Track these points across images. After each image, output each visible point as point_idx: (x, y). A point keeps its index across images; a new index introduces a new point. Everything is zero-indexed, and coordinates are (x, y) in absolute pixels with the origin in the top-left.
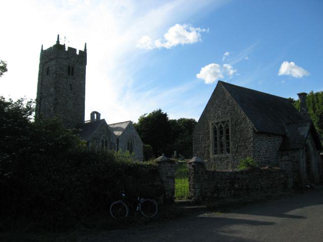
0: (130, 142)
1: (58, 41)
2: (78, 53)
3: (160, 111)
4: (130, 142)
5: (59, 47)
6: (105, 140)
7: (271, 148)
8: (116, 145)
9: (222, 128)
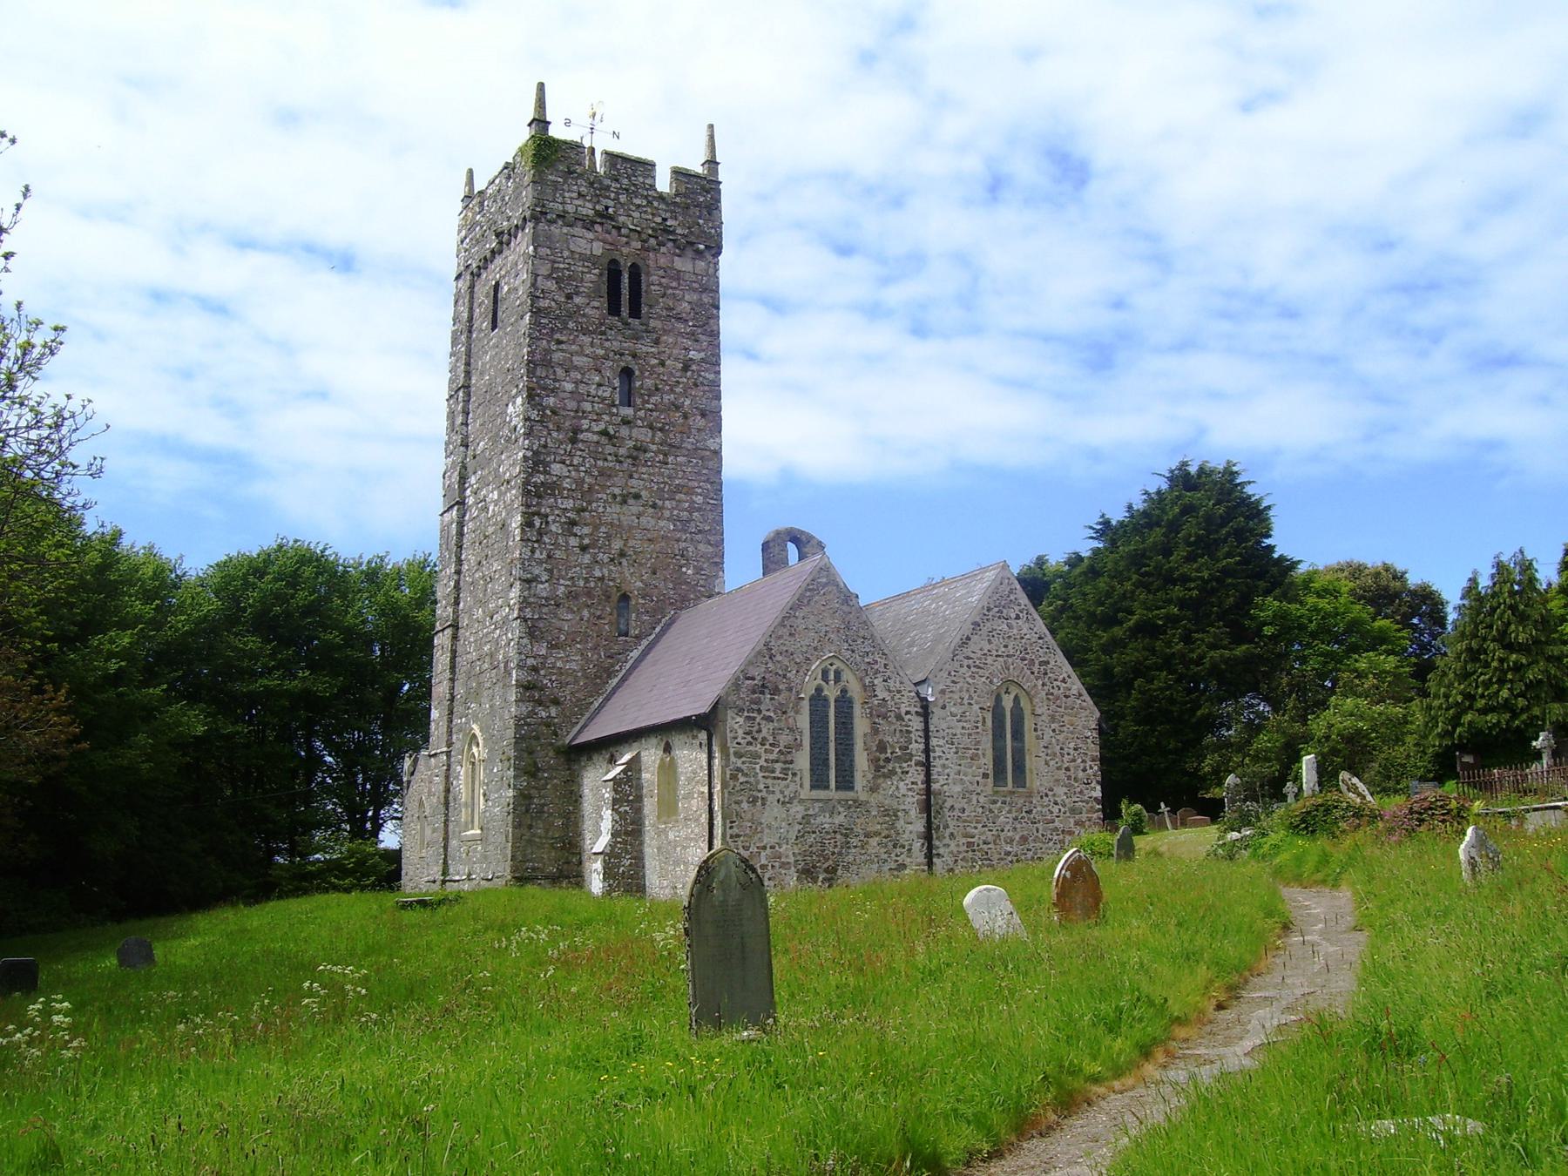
0: (1008, 702)
1: (540, 122)
2: (663, 183)
3: (118, 535)
4: (1008, 702)
5: (548, 154)
6: (831, 692)
8: (916, 724)
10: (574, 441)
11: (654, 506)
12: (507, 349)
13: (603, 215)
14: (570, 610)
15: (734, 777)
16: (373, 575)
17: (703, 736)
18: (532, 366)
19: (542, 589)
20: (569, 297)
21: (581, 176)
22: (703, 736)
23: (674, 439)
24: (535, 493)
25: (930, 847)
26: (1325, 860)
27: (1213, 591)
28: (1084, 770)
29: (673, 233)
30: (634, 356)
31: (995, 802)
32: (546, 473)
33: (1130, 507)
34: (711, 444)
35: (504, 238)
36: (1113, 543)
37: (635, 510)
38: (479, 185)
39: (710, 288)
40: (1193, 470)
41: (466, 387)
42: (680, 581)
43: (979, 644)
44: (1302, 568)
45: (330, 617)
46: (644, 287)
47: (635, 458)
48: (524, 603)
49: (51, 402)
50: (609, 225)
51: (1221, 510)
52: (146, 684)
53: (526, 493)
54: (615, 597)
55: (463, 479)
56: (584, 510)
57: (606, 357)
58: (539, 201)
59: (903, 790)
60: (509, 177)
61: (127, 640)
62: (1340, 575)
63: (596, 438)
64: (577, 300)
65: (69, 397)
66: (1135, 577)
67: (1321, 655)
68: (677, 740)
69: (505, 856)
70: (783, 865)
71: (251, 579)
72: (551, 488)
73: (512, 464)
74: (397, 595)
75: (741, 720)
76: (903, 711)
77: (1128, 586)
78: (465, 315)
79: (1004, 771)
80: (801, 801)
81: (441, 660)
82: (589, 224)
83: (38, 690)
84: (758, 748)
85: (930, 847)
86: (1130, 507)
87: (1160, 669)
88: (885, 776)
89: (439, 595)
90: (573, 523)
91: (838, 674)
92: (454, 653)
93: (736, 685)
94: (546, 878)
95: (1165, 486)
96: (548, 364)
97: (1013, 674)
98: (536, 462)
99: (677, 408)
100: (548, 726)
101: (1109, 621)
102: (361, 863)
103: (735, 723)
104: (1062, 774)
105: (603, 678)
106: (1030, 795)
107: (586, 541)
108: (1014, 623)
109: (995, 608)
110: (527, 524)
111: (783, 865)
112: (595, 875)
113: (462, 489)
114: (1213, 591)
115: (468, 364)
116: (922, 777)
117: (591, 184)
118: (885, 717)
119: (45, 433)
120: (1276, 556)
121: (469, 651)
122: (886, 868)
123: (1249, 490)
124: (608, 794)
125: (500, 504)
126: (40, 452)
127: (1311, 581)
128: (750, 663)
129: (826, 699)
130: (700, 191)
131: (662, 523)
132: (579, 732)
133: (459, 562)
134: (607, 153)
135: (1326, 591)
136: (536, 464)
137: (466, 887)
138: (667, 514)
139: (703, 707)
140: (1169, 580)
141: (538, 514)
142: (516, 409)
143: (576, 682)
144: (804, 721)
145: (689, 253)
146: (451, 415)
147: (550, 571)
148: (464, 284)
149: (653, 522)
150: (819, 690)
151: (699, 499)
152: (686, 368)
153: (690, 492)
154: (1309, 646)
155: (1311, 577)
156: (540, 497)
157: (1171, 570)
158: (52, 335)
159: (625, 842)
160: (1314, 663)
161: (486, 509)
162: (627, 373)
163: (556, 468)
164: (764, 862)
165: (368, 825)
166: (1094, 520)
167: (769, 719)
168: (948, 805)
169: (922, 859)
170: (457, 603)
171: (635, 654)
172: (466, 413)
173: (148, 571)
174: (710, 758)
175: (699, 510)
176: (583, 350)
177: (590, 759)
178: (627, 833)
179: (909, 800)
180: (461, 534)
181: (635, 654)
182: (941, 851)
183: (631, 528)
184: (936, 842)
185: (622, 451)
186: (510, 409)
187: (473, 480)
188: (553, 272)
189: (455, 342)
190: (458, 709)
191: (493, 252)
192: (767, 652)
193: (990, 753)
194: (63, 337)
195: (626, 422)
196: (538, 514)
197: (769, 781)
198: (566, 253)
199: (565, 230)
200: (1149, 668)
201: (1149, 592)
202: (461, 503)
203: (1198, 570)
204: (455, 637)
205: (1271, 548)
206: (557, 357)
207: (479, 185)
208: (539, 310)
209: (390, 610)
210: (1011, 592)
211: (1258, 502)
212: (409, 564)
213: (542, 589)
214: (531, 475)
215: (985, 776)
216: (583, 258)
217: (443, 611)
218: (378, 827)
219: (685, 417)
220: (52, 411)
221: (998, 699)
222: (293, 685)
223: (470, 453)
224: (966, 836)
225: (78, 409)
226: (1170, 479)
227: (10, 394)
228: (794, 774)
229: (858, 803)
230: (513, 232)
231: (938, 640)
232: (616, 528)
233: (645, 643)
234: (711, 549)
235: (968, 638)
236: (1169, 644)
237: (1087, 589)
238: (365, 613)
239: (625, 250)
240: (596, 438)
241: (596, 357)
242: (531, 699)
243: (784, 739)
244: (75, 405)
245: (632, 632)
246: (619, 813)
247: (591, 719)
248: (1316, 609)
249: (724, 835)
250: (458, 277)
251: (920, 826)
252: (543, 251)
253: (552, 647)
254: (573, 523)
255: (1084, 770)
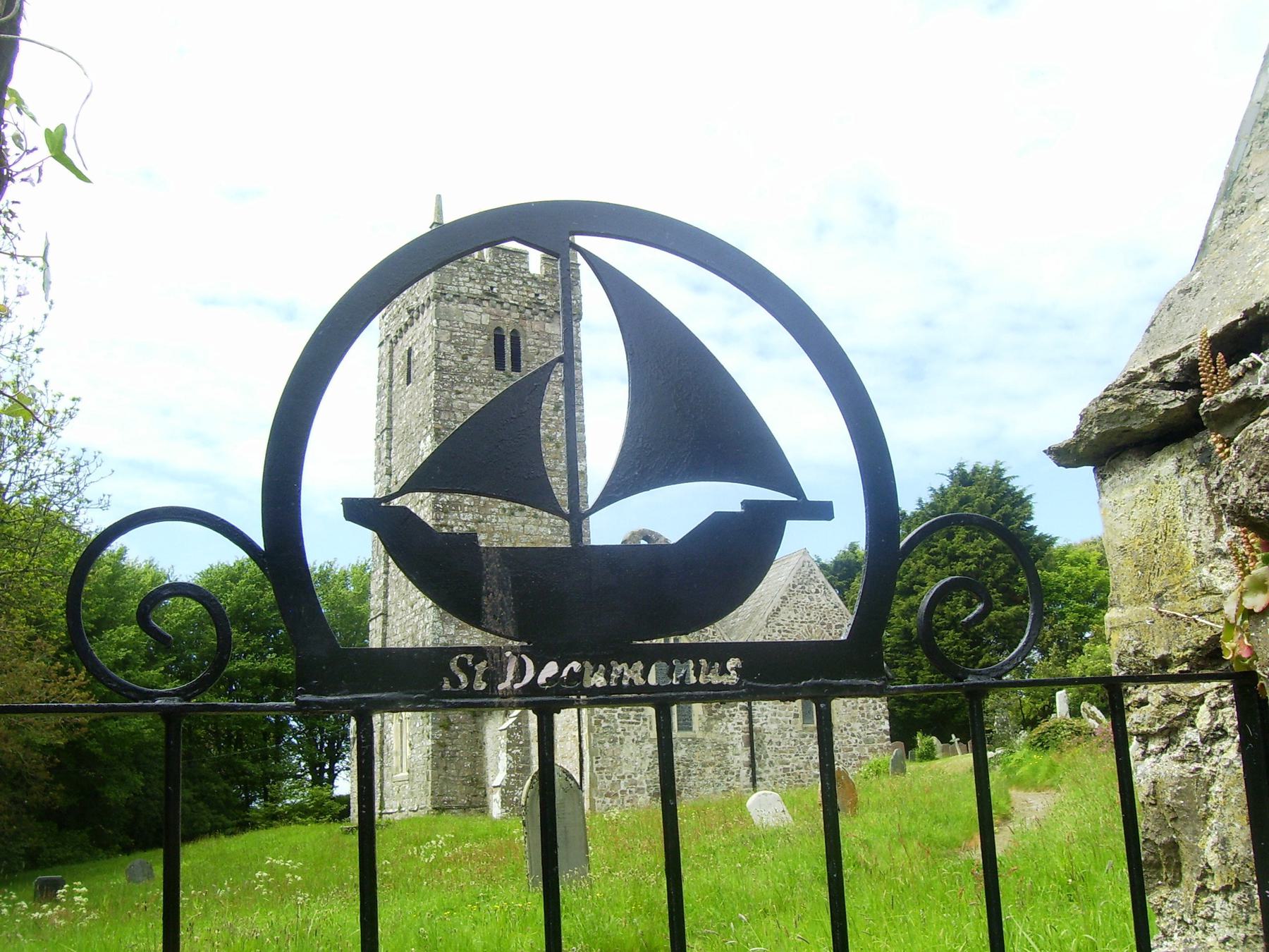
13: (490, 294)
15: (598, 723)
20: (465, 358)
25: (754, 773)
26: (1052, 768)
27: (987, 565)
28: (875, 709)
29: (544, 304)
31: (804, 736)
37: (520, 519)
40: (969, 469)
41: (389, 429)
44: (1059, 543)
46: (522, 348)
49: (71, 454)
51: (991, 500)
52: (147, 667)
56: (480, 521)
59: (731, 729)
61: (132, 633)
62: (1093, 547)
64: (471, 360)
65: (84, 450)
66: (926, 556)
67: (1077, 611)
69: (426, 792)
70: (638, 790)
71: (229, 583)
74: (343, 591)
77: (921, 563)
82: (478, 301)
83: (64, 673)
85: (754, 773)
86: (920, 501)
87: (948, 629)
88: (715, 718)
89: (372, 591)
94: (459, 808)
95: (946, 483)
99: (551, 440)
102: (319, 804)
104: (857, 712)
108: (814, 596)
111: (638, 790)
112: (495, 804)
114: (987, 565)
115: (390, 411)
116: (746, 718)
119: (66, 477)
120: (1037, 534)
122: (720, 790)
123: (1012, 483)
124: (504, 741)
126: (63, 492)
127: (1066, 553)
131: (542, 529)
135: (1078, 560)
137: (398, 817)
138: (545, 522)
140: (953, 558)
149: (535, 528)
154: (1066, 604)
155: (1065, 552)
156: (446, 513)
157: (954, 550)
158: (72, 404)
159: (518, 778)
160: (1071, 617)
164: (623, 788)
165: (326, 775)
168: (767, 739)
169: (748, 782)
170: (386, 596)
173: (148, 579)
177: (490, 713)
178: (518, 770)
179: (736, 736)
182: (763, 776)
183: (517, 534)
184: (758, 769)
186: (422, 445)
189: (379, 395)
191: (406, 325)
194: (78, 405)
197: (626, 726)
198: (462, 324)
199: (460, 306)
201: (938, 567)
203: (975, 548)
204: (385, 623)
205: (1032, 529)
206: (457, 404)
208: (442, 369)
210: (811, 572)
211: (1022, 492)
215: (796, 716)
216: (475, 327)
217: (375, 603)
218: (333, 776)
220: (71, 461)
222: (265, 666)
223: (393, 480)
224: (782, 763)
225: (91, 459)
226: (952, 477)
227: (41, 449)
228: (645, 720)
229: (696, 741)
230: (420, 310)
235: (778, 609)
236: (954, 608)
239: (507, 320)
244: (88, 456)
246: (512, 755)
248: (1070, 575)
249: (591, 767)
251: (745, 757)
252: (444, 323)
255: (875, 709)
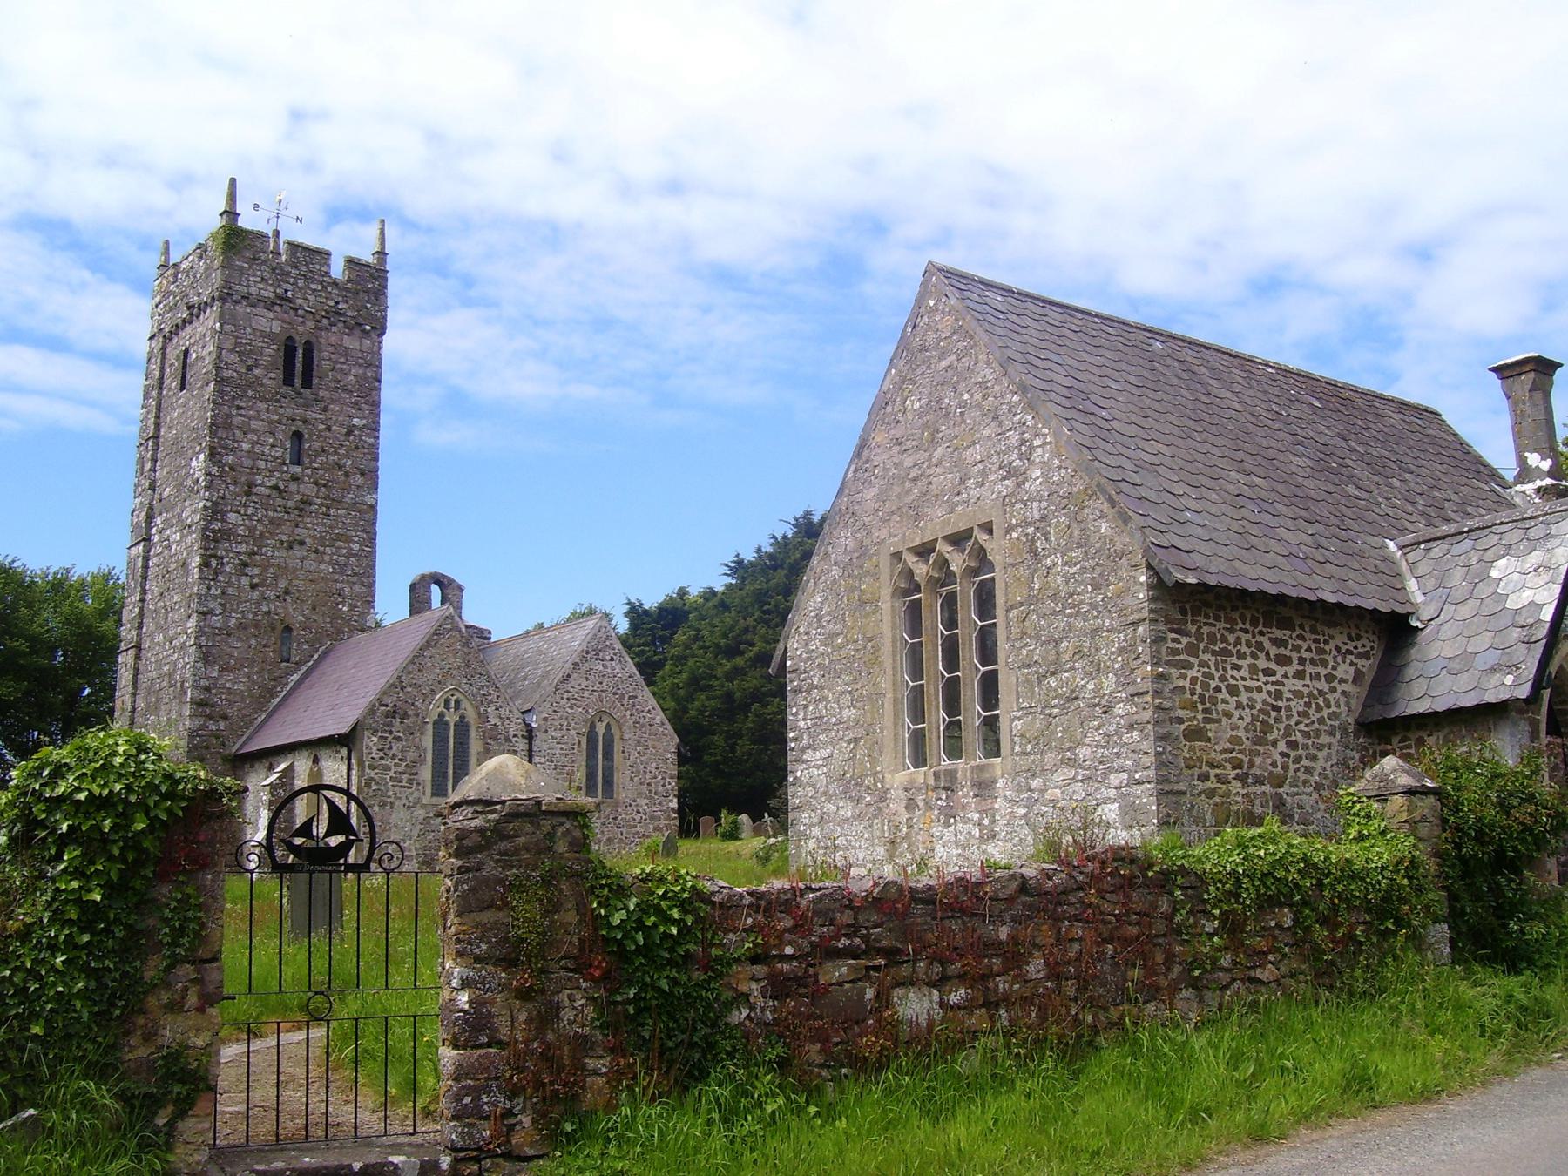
0: (601, 729)
1: (231, 214)
2: (337, 270)
4: (601, 729)
5: (235, 241)
6: (452, 718)
7: (1297, 705)
9: (950, 577)
10: (248, 494)
11: (316, 552)
12: (191, 410)
13: (283, 298)
14: (239, 639)
15: (368, 785)
16: (59, 586)
17: (344, 751)
18: (214, 427)
19: (216, 620)
20: (249, 369)
21: (264, 262)
22: (344, 751)
23: (336, 494)
24: (213, 537)
30: (305, 422)
32: (223, 521)
33: (759, 549)
34: (369, 499)
35: (195, 311)
36: (743, 579)
37: (299, 554)
38: (175, 258)
39: (373, 363)
41: (156, 437)
42: (336, 616)
43: (577, 682)
45: (16, 626)
47: (301, 510)
48: (200, 632)
50: (287, 306)
53: (205, 538)
54: (280, 628)
55: (150, 518)
56: (255, 554)
57: (279, 422)
58: (227, 284)
60: (201, 258)
63: (267, 491)
68: (324, 753)
72: (228, 534)
73: (193, 511)
75: (375, 739)
76: (511, 733)
78: (157, 373)
79: (596, 785)
80: (424, 806)
81: (124, 677)
82: (269, 306)
84: (388, 762)
86: (759, 549)
90: (245, 565)
91: (457, 702)
92: (136, 670)
93: (372, 710)
96: (228, 426)
97: (606, 706)
98: (215, 511)
99: (340, 467)
100: (217, 737)
101: (732, 652)
103: (371, 741)
105: (269, 697)
106: (617, 804)
107: (256, 580)
109: (595, 650)
110: (205, 564)
113: (149, 527)
115: (158, 417)
117: (273, 270)
118: (495, 739)
121: (150, 672)
125: (181, 543)
128: (385, 693)
129: (447, 723)
130: (369, 280)
131: (323, 567)
132: (245, 743)
133: (144, 591)
134: (289, 243)
136: (215, 513)
138: (327, 558)
139: (343, 728)
141: (215, 556)
142: (199, 463)
143: (243, 700)
144: (428, 741)
145: (357, 332)
146: (141, 461)
147: (223, 605)
148: (157, 345)
150: (441, 715)
151: (356, 547)
152: (349, 433)
153: (349, 540)
161: (169, 547)
162: (297, 436)
163: (232, 517)
166: (730, 558)
167: (399, 739)
170: (140, 627)
171: (295, 677)
172: (154, 460)
174: (349, 769)
175: (355, 555)
176: (258, 416)
177: (252, 766)
180: (146, 567)
181: (295, 677)
183: (295, 570)
185: (290, 504)
186: (194, 463)
187: (159, 520)
188: (231, 338)
189: (146, 396)
190: (139, 720)
192: (398, 685)
193: (583, 770)
195: (295, 479)
196: (215, 556)
198: (249, 330)
200: (765, 695)
202: (147, 539)
204: (138, 657)
206: (238, 420)
207: (175, 258)
209: (76, 620)
212: (93, 576)
213: (216, 620)
214: (210, 522)
216: (264, 335)
217: (127, 633)
219: (347, 475)
221: (593, 726)
230: (203, 307)
231: (545, 676)
232: (283, 569)
233: (304, 668)
234: (364, 590)
237: (716, 621)
238: (49, 621)
239: (301, 329)
240: (267, 491)
241: (270, 422)
242: (203, 715)
243: (411, 755)
245: (293, 659)
247: (255, 732)
250: (151, 338)
252: (229, 328)
253: (222, 670)
254: (245, 565)
